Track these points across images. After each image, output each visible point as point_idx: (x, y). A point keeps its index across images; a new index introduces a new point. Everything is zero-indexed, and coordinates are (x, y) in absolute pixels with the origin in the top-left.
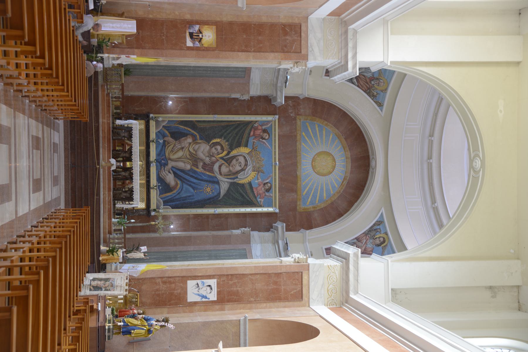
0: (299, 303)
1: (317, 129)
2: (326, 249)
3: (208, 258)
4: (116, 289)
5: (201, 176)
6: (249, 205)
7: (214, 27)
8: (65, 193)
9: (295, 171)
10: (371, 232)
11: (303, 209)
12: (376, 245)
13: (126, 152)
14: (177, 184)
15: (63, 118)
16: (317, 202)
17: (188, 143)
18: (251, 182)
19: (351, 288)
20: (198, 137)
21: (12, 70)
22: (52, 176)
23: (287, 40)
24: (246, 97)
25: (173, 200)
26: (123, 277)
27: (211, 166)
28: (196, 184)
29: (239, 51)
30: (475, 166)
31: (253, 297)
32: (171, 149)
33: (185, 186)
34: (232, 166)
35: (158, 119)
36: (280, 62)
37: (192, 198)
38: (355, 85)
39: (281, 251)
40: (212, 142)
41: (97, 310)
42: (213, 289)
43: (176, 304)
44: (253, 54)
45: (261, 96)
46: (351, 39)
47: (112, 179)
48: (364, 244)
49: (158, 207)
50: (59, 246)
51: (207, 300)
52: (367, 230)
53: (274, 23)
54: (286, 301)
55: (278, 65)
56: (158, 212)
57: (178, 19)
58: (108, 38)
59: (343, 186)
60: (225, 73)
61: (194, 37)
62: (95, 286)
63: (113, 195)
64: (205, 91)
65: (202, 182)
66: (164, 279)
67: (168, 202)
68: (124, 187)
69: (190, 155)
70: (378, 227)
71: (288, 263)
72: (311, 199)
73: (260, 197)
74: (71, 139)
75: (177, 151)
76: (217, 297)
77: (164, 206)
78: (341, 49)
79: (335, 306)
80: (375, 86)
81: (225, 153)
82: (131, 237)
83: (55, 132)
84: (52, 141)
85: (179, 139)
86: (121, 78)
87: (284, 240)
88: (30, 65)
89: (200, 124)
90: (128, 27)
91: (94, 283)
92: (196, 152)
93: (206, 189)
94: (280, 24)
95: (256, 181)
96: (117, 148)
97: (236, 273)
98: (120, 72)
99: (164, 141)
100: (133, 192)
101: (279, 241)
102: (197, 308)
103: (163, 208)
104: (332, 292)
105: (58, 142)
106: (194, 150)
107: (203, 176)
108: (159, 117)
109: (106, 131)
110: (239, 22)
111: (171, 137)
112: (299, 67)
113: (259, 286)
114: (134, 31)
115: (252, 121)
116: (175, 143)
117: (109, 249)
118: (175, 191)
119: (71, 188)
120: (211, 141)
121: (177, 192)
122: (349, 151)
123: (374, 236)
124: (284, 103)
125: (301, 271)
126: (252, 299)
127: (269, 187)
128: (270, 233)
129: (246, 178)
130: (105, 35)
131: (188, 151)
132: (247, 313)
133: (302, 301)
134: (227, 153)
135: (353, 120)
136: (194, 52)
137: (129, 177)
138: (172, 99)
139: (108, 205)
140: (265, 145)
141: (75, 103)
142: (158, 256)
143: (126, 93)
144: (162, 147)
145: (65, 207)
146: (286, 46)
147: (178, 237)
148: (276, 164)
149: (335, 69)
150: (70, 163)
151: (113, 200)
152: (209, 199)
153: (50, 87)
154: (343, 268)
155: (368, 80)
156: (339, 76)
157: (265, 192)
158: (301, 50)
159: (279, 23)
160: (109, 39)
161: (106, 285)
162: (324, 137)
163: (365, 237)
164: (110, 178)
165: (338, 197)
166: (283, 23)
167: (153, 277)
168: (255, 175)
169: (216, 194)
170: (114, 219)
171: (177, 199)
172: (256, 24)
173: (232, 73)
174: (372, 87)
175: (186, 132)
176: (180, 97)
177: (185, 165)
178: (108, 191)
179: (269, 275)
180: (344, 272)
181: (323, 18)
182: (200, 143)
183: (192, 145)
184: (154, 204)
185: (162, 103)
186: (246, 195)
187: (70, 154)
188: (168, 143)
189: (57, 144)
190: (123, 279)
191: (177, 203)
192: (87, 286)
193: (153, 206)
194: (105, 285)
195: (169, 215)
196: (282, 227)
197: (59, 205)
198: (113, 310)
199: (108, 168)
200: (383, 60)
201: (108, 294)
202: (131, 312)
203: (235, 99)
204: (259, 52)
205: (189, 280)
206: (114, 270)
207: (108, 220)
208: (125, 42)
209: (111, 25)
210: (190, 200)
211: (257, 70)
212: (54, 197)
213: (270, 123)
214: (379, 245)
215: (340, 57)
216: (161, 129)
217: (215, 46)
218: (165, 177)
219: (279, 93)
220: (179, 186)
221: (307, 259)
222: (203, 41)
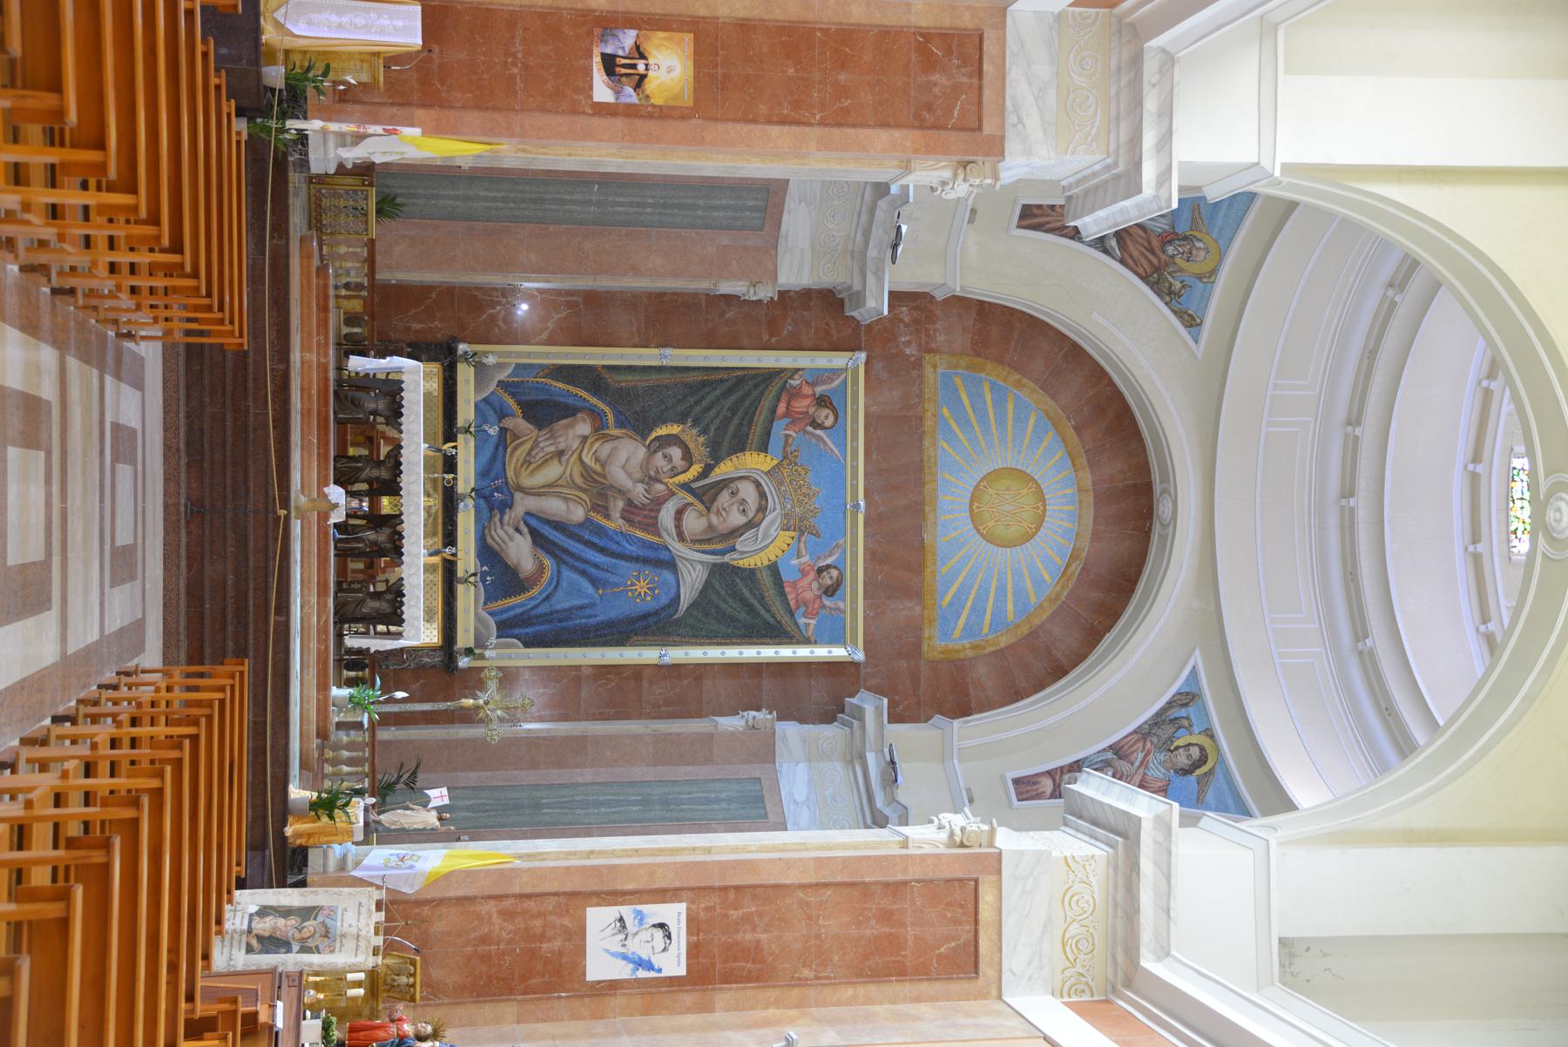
0: (966, 986)
1: (988, 397)
2: (1017, 782)
3: (640, 808)
4: (342, 945)
5: (617, 543)
6: (771, 638)
7: (688, 38)
8: (165, 605)
9: (918, 530)
10: (1159, 727)
11: (940, 652)
12: (1176, 771)
13: (379, 464)
14: (541, 568)
15: (160, 334)
16: (986, 630)
17: (580, 436)
18: (776, 563)
19: (1146, 937)
20: (610, 417)
21: (75, 256)
22: (107, 547)
23: (935, 85)
24: (765, 293)
25: (529, 619)
26: (364, 901)
27: (651, 510)
28: (603, 570)
29: (769, 122)
30: (1554, 524)
31: (810, 966)
32: (524, 454)
33: (567, 574)
34: (718, 513)
35: (485, 360)
36: (909, 161)
37: (588, 612)
38: (1113, 258)
39: (874, 786)
40: (654, 435)
41: (271, 1027)
42: (674, 936)
43: (548, 989)
44: (817, 132)
45: (811, 289)
46: (1154, 85)
47: (332, 552)
48: (1139, 767)
49: (480, 642)
50: (206, 711)
51: (652, 974)
52: (1145, 723)
53: (892, 27)
54: (922, 980)
55: (899, 171)
56: (482, 657)
57: (564, 9)
58: (323, 65)
59: (1068, 579)
60: (699, 213)
61: (618, 69)
62: (267, 934)
63: (335, 608)
64: (636, 271)
65: (623, 563)
66: (507, 903)
67: (511, 627)
68: (372, 579)
69: (585, 474)
70: (1183, 712)
71: (928, 850)
72: (968, 619)
73: (805, 611)
74: (188, 417)
75: (543, 463)
76: (688, 965)
77: (498, 637)
78: (1118, 118)
79: (1086, 998)
80: (1178, 260)
81: (696, 469)
82: (391, 738)
83: (127, 390)
84: (109, 419)
85: (551, 423)
86: (367, 222)
87: (882, 751)
88: (122, 241)
89: (617, 377)
90: (394, 27)
91: (264, 926)
92: (603, 466)
93: (633, 584)
94: (912, 30)
95: (794, 562)
96: (352, 451)
97: (753, 881)
98: (362, 204)
99: (503, 431)
100: (404, 595)
101: (868, 754)
102: (619, 1001)
103: (497, 646)
104: (1078, 948)
105: (135, 423)
106: (597, 460)
107: (625, 543)
108: (485, 354)
109: (314, 392)
110: (772, 21)
111: (523, 417)
112: (972, 181)
113: (830, 925)
114: (416, 40)
115: (782, 371)
116: (538, 436)
117: (319, 797)
118: (534, 592)
119: (188, 585)
120: (651, 430)
121: (540, 593)
122: (1088, 470)
123: (1171, 740)
124: (886, 313)
125: (975, 876)
126: (806, 973)
127: (835, 579)
128: (838, 730)
129: (762, 549)
130: (314, 52)
131: (578, 462)
132: (791, 1021)
133: (977, 978)
134: (700, 470)
135: (1102, 370)
136: (619, 123)
137: (389, 546)
138: (529, 296)
139: (318, 641)
140: (822, 446)
141: (219, 315)
142: (479, 802)
143: (381, 276)
144: (497, 449)
145: (164, 660)
146: (929, 107)
147: (544, 738)
148: (856, 506)
149: (1087, 192)
150: (183, 501)
151: (335, 623)
152: (646, 616)
153: (143, 258)
154: (1116, 868)
155: (1155, 243)
156: (1101, 213)
157: (820, 597)
158: (980, 120)
159: (907, 27)
160: (328, 67)
161: (306, 934)
162: (1010, 422)
163: (1140, 744)
164: (328, 551)
165: (1054, 614)
166: (922, 28)
167: (469, 894)
168: (790, 541)
169: (664, 601)
170: (339, 687)
171: (540, 616)
172: (830, 29)
173: (722, 214)
174: (1167, 265)
175: (572, 402)
176: (555, 290)
177: (568, 507)
178: (319, 596)
179: (865, 889)
180: (1120, 882)
181: (1056, 12)
182: (618, 438)
183: (592, 444)
184: (466, 631)
185: (498, 308)
186: (762, 605)
187: (183, 469)
188: (516, 437)
189: (133, 432)
190: (363, 910)
191: (542, 628)
192: (236, 936)
193: (464, 639)
194: (300, 931)
195: (517, 668)
196: (878, 709)
197: (139, 648)
198: (326, 1028)
199: (318, 516)
200: (1256, 161)
201: (311, 965)
202: (393, 1029)
203: (729, 299)
204: (839, 125)
205: (591, 906)
206: (334, 872)
207: (318, 691)
208: (382, 79)
209: (334, 18)
210: (584, 621)
211: (803, 204)
212: (113, 626)
213: (839, 376)
214: (1186, 772)
215: (1112, 146)
216: (492, 393)
217: (691, 104)
218: (504, 547)
219: (871, 281)
220: (547, 575)
221: (992, 832)
222: (650, 86)
